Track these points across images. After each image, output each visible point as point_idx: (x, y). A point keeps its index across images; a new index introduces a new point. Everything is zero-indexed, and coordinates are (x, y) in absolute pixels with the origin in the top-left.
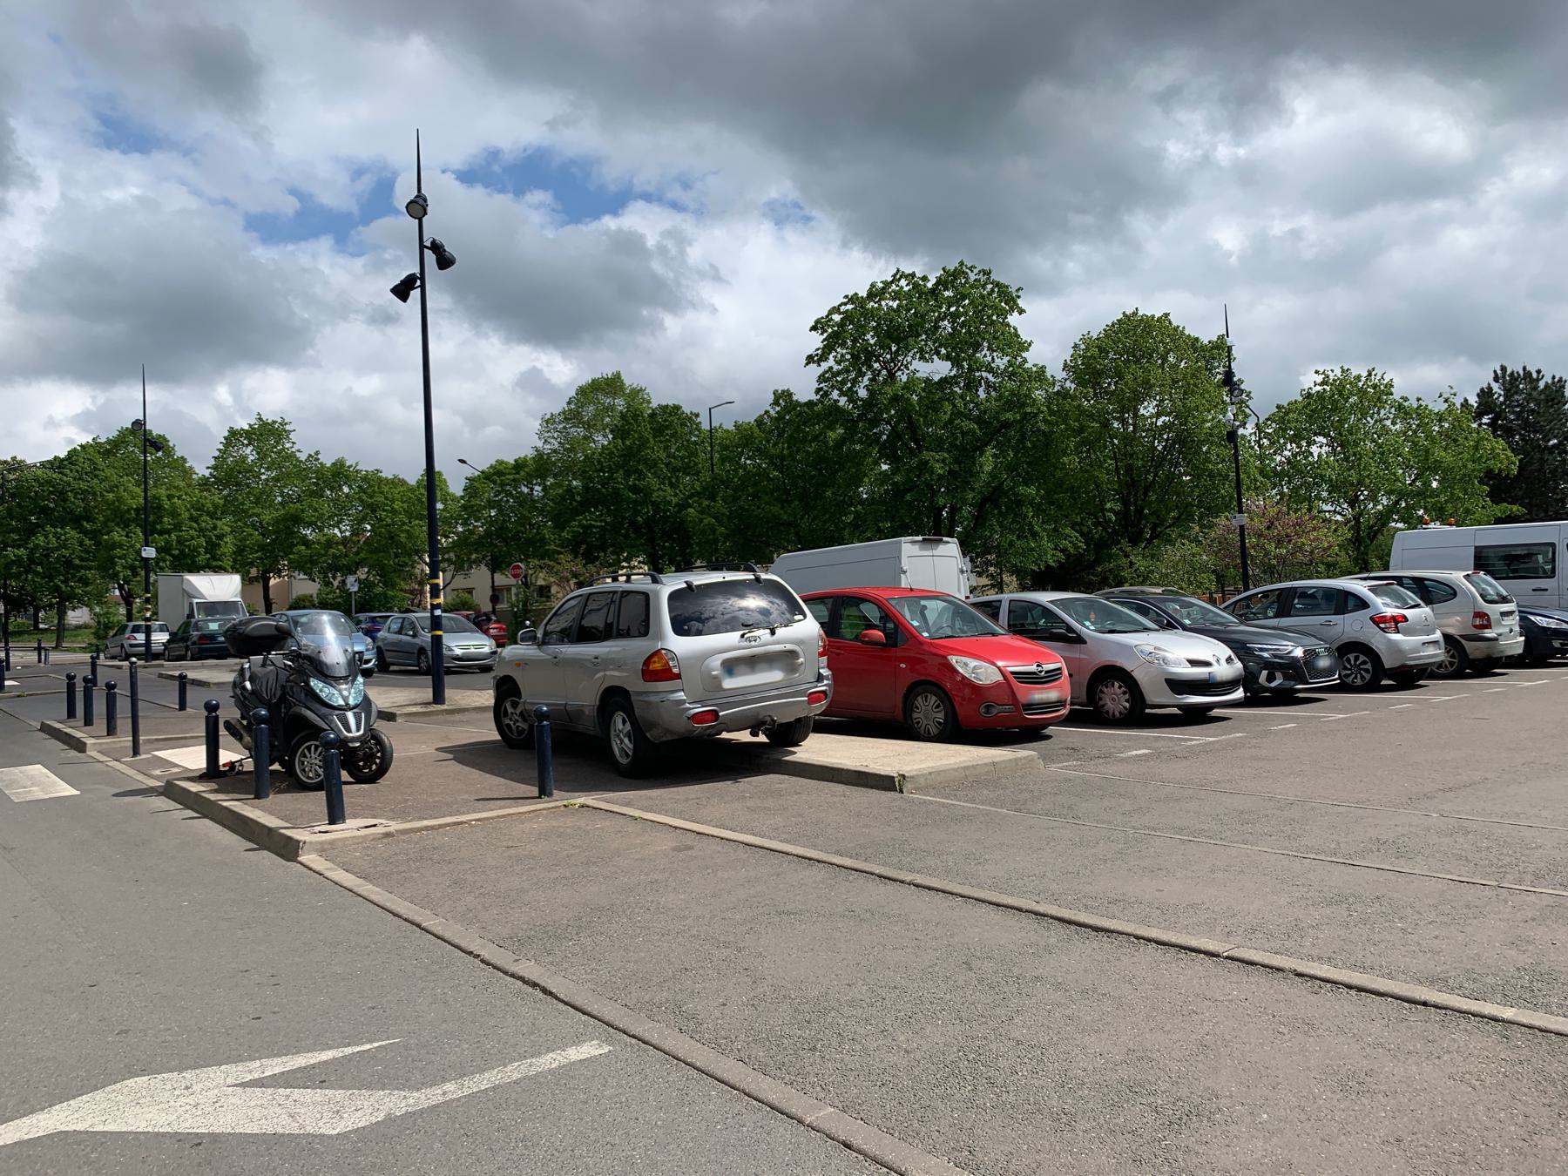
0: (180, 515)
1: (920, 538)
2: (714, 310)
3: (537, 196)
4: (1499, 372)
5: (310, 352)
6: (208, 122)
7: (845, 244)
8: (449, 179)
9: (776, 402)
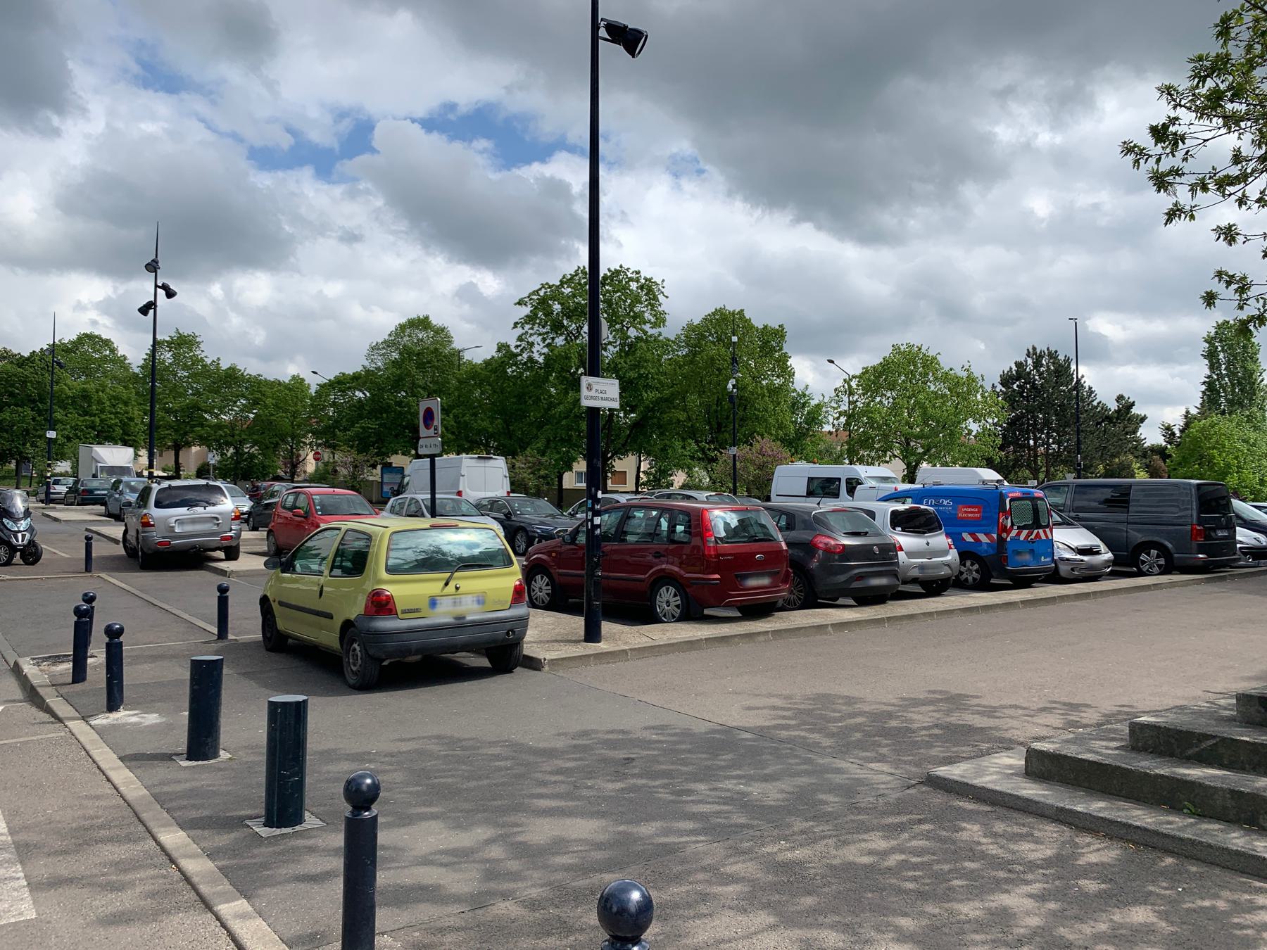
0: (104, 403)
1: (476, 456)
2: (620, 245)
3: (482, 144)
4: (1031, 350)
5: (292, 260)
6: (231, 73)
7: (730, 194)
8: (416, 129)
9: (499, 350)
